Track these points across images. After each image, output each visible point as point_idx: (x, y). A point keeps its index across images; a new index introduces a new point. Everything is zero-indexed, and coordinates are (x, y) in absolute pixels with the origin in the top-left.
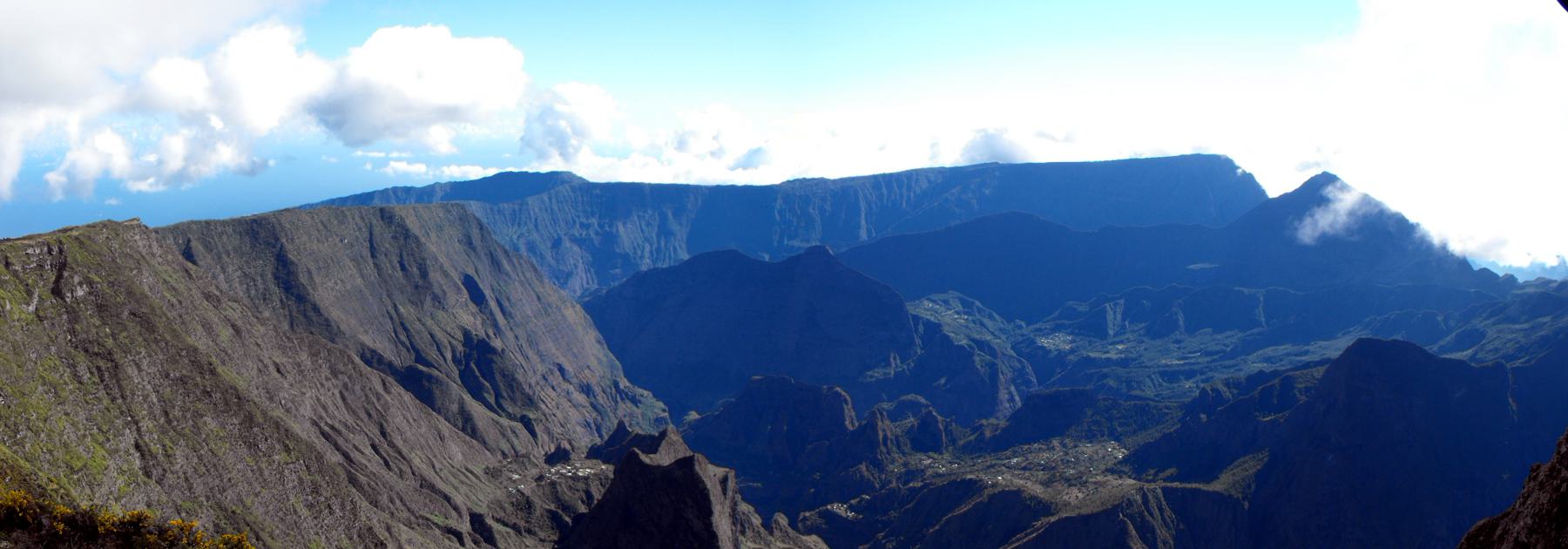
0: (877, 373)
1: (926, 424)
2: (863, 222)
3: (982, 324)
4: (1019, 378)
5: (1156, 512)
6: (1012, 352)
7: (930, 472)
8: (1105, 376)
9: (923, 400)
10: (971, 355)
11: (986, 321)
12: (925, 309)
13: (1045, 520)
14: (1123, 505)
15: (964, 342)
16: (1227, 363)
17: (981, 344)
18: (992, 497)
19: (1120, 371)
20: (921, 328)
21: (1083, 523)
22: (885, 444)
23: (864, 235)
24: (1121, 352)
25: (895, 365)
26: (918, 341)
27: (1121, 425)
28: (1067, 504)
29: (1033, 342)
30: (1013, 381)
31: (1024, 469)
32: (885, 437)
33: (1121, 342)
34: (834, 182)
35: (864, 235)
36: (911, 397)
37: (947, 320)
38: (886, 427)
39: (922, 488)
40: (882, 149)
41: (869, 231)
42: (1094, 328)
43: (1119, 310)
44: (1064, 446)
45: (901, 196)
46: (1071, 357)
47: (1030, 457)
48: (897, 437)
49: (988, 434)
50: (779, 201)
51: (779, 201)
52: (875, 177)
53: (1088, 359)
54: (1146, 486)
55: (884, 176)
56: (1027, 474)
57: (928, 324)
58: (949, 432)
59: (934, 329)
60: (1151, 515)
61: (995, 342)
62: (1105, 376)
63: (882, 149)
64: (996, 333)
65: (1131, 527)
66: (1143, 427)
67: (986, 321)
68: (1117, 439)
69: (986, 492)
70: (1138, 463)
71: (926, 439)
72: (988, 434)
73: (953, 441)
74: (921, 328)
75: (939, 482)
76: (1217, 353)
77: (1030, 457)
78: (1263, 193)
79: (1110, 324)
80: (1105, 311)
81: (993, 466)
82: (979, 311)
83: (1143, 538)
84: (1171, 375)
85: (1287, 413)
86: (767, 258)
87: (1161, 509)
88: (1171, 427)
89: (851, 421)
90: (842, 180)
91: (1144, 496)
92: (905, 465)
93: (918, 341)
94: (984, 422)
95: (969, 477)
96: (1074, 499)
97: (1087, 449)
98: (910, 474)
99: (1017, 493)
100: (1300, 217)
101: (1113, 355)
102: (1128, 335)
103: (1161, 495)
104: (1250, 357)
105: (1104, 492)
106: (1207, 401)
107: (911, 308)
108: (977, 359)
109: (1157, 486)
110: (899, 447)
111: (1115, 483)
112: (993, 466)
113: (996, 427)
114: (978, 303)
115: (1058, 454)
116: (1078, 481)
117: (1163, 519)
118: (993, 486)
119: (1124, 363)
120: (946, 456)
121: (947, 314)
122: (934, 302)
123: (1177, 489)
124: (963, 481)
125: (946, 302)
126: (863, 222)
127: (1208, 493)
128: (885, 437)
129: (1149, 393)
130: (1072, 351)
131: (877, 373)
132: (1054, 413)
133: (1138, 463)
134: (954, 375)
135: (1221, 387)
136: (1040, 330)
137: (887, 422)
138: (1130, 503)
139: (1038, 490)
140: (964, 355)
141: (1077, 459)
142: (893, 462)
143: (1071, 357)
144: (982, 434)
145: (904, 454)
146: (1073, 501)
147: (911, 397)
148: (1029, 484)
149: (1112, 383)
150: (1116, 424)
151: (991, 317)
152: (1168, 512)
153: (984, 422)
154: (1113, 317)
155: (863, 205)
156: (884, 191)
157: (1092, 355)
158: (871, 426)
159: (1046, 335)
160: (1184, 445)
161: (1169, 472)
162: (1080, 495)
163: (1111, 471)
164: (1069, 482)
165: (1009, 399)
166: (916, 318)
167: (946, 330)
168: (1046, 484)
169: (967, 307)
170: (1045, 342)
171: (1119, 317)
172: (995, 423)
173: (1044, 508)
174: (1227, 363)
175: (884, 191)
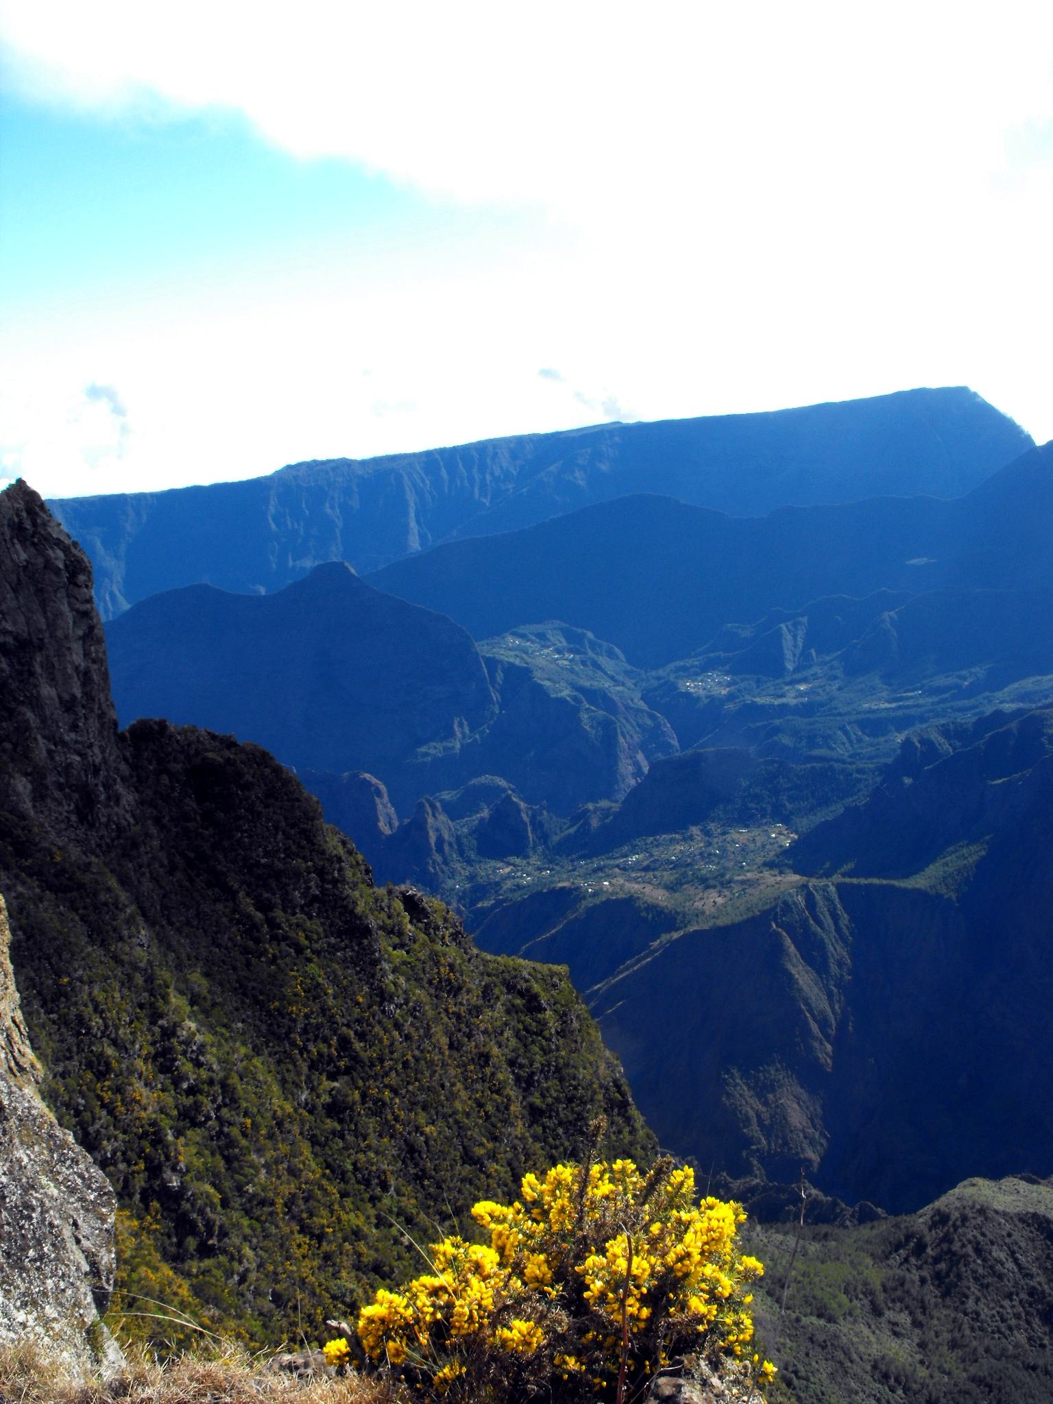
0: (434, 749)
1: (504, 816)
2: (413, 524)
3: (597, 666)
4: (652, 740)
5: (828, 921)
6: (642, 705)
7: (509, 884)
8: (777, 730)
9: (503, 783)
10: (576, 710)
11: (603, 661)
12: (509, 649)
13: (665, 937)
14: (780, 910)
15: (566, 693)
16: (959, 703)
17: (595, 696)
18: (591, 911)
19: (800, 722)
20: (500, 677)
21: (721, 937)
22: (440, 849)
23: (414, 544)
24: (801, 694)
25: (461, 735)
26: (495, 696)
27: (792, 799)
28: (699, 914)
29: (673, 687)
30: (643, 747)
31: (646, 869)
32: (440, 841)
33: (805, 680)
34: (363, 463)
35: (414, 544)
36: (485, 779)
37: (541, 662)
38: (439, 825)
39: (493, 907)
40: (547, 373)
41: (422, 537)
42: (762, 662)
43: (801, 634)
44: (707, 833)
45: (471, 480)
46: (730, 706)
47: (656, 852)
48: (458, 839)
49: (595, 823)
50: (273, 502)
51: (273, 502)
52: (429, 454)
53: (754, 706)
54: (813, 882)
55: (442, 452)
56: (651, 874)
57: (510, 669)
58: (537, 825)
59: (519, 676)
60: (819, 922)
61: (614, 690)
62: (777, 730)
63: (547, 373)
64: (616, 678)
65: (788, 941)
66: (825, 802)
67: (603, 661)
68: (786, 820)
69: (584, 904)
70: (800, 858)
71: (501, 838)
72: (595, 823)
73: (544, 838)
74: (500, 677)
75: (517, 896)
76: (949, 688)
77: (656, 852)
78: (1028, 439)
79: (788, 655)
80: (779, 635)
81: (600, 869)
82: (593, 645)
83: (808, 959)
84: (874, 726)
85: (1028, 772)
86: (263, 591)
87: (835, 917)
88: (861, 799)
89: (387, 818)
90: (376, 461)
91: (810, 899)
92: (471, 878)
93: (495, 696)
94: (590, 806)
95: (560, 885)
96: (711, 906)
97: (741, 835)
98: (480, 889)
99: (629, 902)
100: (538, 692)
101: (790, 700)
102: (816, 669)
103: (835, 896)
104: (999, 694)
105: (754, 896)
106: (909, 759)
107: (484, 649)
108: (584, 716)
109: (830, 885)
110: (461, 852)
111: (771, 880)
112: (600, 869)
113: (606, 812)
114: (590, 635)
115: (698, 845)
116: (720, 882)
117: (838, 929)
118: (594, 895)
119: (807, 710)
120: (535, 860)
121: (545, 657)
122: (523, 636)
123: (859, 886)
124: (553, 892)
125: (542, 636)
126: (413, 524)
127: (905, 891)
128: (440, 841)
129: (842, 751)
130: (731, 697)
131: (434, 749)
132: (683, 797)
133: (800, 858)
134: (552, 743)
135: (936, 737)
136: (685, 669)
137: (443, 817)
138: (787, 907)
139: (660, 897)
140: (567, 711)
141: (723, 850)
142: (453, 875)
143: (730, 706)
144: (587, 823)
145: (469, 862)
146: (709, 909)
147: (485, 779)
148: (648, 889)
149: (786, 740)
150: (784, 798)
151: (611, 654)
152: (845, 918)
153: (590, 806)
154: (791, 643)
155: (411, 499)
156: (444, 473)
157: (759, 700)
158: (419, 826)
159: (693, 676)
160: (871, 828)
161: (850, 866)
162: (720, 900)
163: (770, 865)
164: (706, 883)
165: (631, 768)
166: (492, 663)
167: (538, 676)
168: (671, 888)
169: (575, 642)
170: (690, 686)
171: (800, 643)
172: (599, 809)
173: (664, 920)
174: (959, 703)
175: (444, 473)
